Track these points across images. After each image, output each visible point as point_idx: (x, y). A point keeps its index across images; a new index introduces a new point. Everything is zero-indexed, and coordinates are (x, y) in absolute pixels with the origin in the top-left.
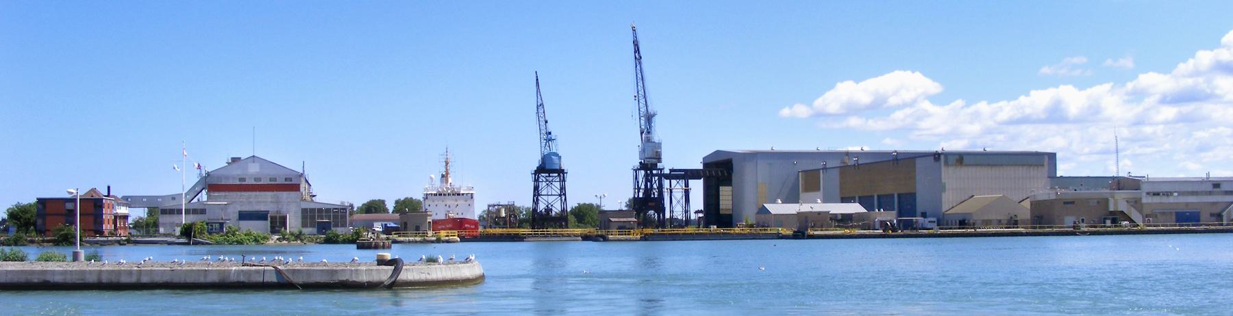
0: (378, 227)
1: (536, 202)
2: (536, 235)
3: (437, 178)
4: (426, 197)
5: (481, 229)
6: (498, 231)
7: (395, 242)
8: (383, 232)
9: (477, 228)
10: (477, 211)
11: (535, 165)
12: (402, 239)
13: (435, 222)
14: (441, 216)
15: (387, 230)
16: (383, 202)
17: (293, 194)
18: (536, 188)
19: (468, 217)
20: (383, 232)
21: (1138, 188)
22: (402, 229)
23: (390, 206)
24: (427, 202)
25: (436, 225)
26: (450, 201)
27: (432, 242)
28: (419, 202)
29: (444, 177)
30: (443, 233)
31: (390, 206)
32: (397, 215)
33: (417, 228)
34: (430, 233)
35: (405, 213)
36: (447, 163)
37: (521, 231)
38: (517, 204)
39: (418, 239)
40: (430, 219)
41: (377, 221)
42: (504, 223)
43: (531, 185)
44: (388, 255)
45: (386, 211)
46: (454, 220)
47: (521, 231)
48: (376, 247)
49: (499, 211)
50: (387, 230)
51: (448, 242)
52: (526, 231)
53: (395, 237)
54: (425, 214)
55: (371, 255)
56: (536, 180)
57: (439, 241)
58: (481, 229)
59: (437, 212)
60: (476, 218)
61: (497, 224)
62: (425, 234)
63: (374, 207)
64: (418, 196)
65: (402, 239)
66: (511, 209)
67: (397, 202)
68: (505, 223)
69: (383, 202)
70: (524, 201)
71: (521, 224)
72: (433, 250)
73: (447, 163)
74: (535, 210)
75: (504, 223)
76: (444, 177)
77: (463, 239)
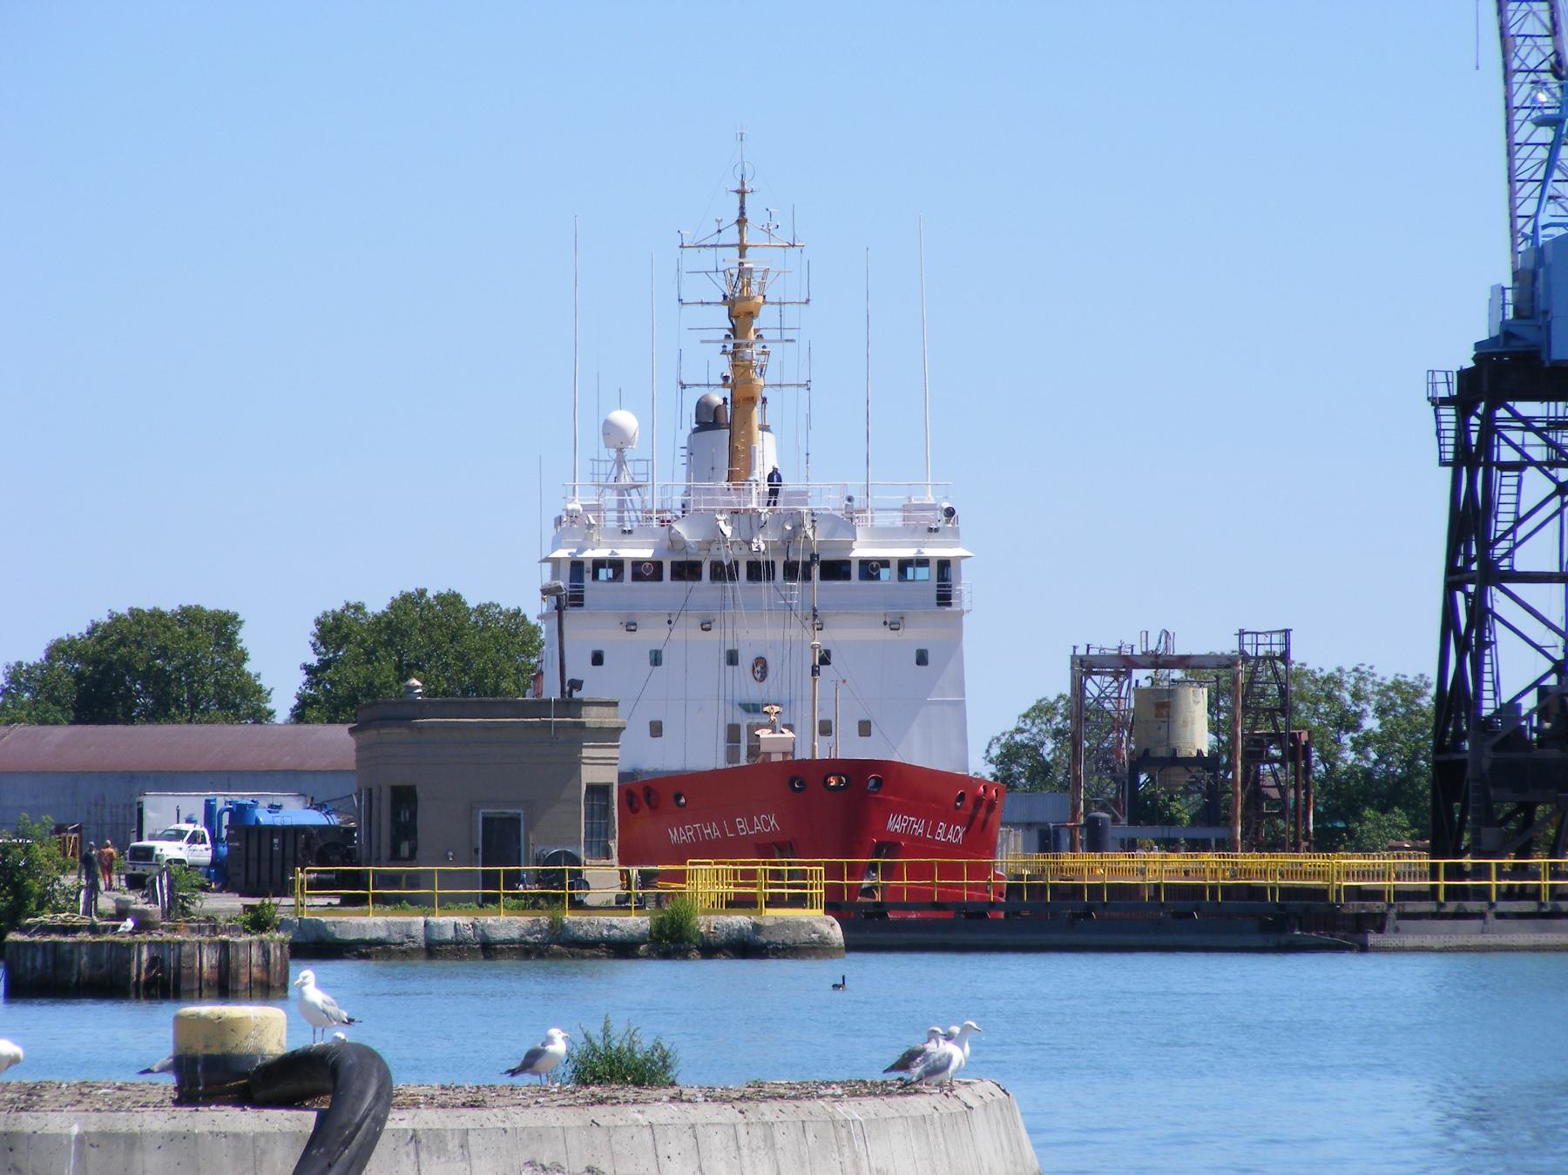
0: (176, 832)
1: (1467, 635)
2: (1457, 902)
3: (659, 434)
4: (573, 587)
5: (1012, 857)
6: (1157, 867)
7: (318, 947)
8: (221, 875)
9: (981, 841)
10: (990, 699)
11: (1461, 330)
12: (371, 922)
13: (647, 796)
14: (695, 749)
15: (253, 859)
16: (223, 627)
17: (612, 709)
18: (1470, 523)
19: (916, 750)
20: (221, 875)
21: (738, 727)
22: (369, 847)
23: (279, 663)
24: (584, 632)
25: (655, 813)
26: (765, 624)
27: (623, 949)
28: (510, 632)
29: (723, 423)
30: (706, 885)
31: (279, 663)
32: (335, 741)
33: (500, 840)
34: (603, 879)
35: (402, 713)
36: (741, 314)
37: (1339, 870)
38: (1315, 655)
39: (506, 923)
40: (599, 768)
41: (173, 780)
42: (1215, 802)
43: (1430, 496)
44: (268, 1028)
45: (239, 699)
46: (801, 776)
47: (1339, 870)
48: (165, 983)
49: (1162, 705)
50: (253, 859)
51: (746, 947)
52: (1389, 865)
53: (315, 908)
54: (565, 723)
55: (141, 1035)
56: (1471, 458)
57: (673, 941)
58: (1012, 857)
59: (663, 710)
60: (980, 767)
61: (1146, 816)
62: (560, 883)
63: (147, 671)
64: (510, 582)
65: (371, 922)
66: (1260, 688)
67: (332, 631)
68: (1212, 813)
69: (223, 627)
70: (1372, 628)
71: (1342, 814)
72: (642, 1002)
73: (741, 314)
74: (1456, 699)
75: (1215, 802)
76: (723, 423)
77: (872, 928)
